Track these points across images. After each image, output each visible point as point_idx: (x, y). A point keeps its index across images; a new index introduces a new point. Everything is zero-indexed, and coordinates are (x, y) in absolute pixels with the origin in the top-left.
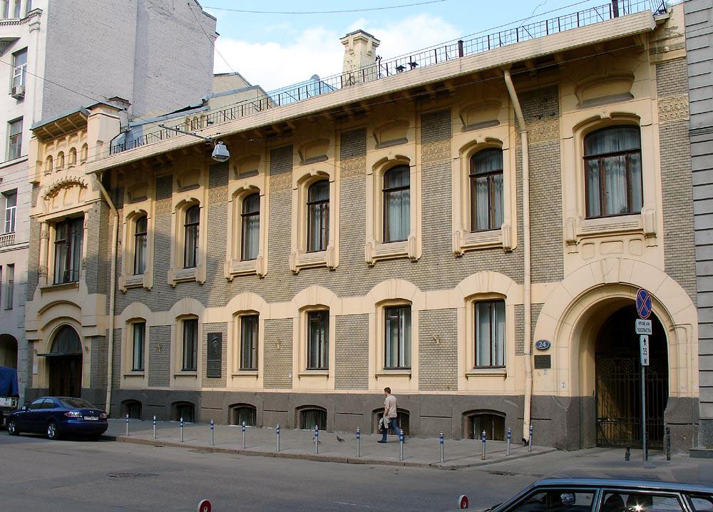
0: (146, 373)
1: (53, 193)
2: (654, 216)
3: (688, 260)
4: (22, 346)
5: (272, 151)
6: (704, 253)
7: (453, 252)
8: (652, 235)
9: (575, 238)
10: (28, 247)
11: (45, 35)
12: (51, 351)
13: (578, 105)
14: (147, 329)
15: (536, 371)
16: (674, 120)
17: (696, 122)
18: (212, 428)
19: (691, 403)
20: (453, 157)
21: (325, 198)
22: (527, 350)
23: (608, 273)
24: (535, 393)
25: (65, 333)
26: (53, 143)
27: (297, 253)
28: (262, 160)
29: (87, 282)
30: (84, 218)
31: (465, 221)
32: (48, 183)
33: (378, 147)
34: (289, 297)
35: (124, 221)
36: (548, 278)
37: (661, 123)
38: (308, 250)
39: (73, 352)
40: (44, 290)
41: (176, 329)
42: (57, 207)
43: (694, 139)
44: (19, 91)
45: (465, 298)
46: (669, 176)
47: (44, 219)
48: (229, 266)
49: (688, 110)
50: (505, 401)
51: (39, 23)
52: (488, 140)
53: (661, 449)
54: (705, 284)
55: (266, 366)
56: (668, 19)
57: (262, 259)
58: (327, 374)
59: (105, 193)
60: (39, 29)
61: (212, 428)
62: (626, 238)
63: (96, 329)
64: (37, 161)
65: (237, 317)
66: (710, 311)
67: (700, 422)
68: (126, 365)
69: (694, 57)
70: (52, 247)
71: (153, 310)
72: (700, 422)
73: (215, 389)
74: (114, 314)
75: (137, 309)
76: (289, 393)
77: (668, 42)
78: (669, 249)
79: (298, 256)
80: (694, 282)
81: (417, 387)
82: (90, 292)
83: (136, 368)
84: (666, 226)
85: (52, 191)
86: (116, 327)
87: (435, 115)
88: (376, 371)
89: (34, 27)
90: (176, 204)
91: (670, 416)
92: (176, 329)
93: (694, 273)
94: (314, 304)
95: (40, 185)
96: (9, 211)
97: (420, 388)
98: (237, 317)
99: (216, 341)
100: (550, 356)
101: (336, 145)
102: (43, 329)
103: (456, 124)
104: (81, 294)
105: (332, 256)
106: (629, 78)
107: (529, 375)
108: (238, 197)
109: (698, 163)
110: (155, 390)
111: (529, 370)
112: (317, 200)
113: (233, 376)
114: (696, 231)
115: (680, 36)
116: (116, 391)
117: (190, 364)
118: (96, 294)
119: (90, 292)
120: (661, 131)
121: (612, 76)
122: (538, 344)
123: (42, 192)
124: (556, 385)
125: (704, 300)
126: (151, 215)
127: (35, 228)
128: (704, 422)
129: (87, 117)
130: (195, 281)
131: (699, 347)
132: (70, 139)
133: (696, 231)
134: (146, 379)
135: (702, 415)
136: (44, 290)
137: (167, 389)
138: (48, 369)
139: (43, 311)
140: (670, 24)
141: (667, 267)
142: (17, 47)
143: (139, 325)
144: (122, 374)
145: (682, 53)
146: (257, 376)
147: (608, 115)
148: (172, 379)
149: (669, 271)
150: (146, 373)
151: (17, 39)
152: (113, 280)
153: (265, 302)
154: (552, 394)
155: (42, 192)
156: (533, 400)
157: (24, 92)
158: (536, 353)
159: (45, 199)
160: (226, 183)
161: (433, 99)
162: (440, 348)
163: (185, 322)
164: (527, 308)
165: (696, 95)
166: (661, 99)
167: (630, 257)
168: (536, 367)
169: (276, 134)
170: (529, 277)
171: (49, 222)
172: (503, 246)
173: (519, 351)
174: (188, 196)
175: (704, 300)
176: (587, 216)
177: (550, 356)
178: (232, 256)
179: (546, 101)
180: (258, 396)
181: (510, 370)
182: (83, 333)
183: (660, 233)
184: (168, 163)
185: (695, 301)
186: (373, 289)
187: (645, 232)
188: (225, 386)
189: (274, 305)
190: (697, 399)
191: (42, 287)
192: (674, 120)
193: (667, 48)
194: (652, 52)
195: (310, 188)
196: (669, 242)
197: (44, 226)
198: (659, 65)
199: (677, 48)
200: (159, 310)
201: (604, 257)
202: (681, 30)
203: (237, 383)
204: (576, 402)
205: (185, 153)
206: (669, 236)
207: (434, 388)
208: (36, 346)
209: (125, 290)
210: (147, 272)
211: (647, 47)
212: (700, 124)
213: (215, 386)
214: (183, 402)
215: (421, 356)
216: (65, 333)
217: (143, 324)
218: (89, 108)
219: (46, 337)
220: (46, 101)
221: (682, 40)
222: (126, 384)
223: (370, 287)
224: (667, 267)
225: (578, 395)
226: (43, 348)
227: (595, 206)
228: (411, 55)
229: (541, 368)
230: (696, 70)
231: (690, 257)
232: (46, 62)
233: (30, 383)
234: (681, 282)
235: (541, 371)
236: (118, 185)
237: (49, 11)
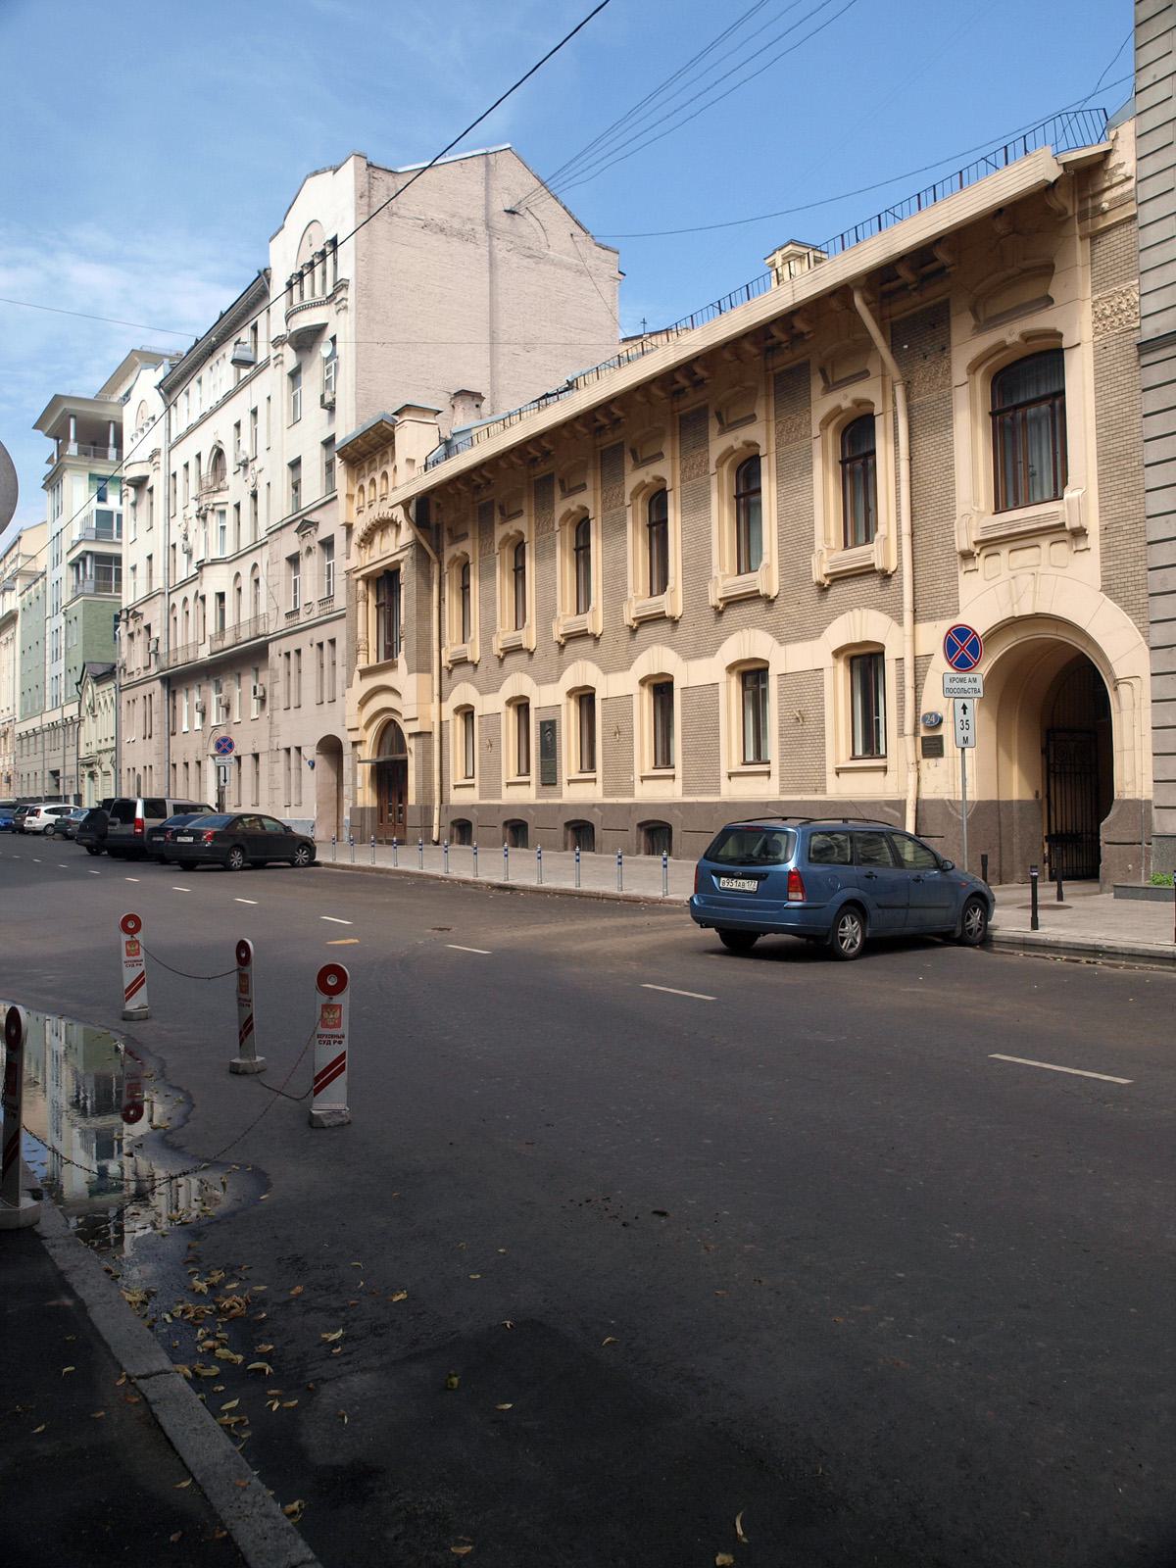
0: (678, 771)
1: (367, 539)
2: (1082, 503)
3: (1137, 568)
4: (347, 749)
5: (681, 418)
6: (1163, 555)
7: (958, 550)
8: (1079, 533)
9: (972, 547)
10: (343, 616)
11: (353, 314)
12: (378, 755)
13: (975, 327)
14: (476, 719)
15: (924, 762)
16: (1116, 331)
17: (1151, 329)
18: (421, 850)
19: (1141, 808)
20: (814, 436)
21: (1056, 389)
22: (909, 728)
23: (1018, 600)
24: (924, 796)
25: (390, 732)
26: (363, 467)
27: (825, 551)
28: (759, 395)
29: (406, 658)
30: (399, 570)
31: (832, 534)
32: (360, 526)
33: (722, 432)
34: (817, 633)
35: (445, 571)
36: (939, 614)
37: (1097, 338)
38: (846, 545)
39: (400, 756)
40: (365, 673)
41: (641, 701)
42: (374, 557)
43: (1147, 359)
44: (328, 399)
45: (568, 693)
46: (1108, 428)
47: (358, 575)
48: (821, 561)
49: (1137, 310)
50: (887, 809)
51: (346, 300)
52: (1027, 337)
53: (1098, 882)
54: (1165, 607)
55: (605, 765)
56: (1107, 154)
57: (768, 566)
58: (767, 769)
59: (418, 533)
60: (345, 308)
61: (421, 850)
62: (1045, 543)
63: (418, 722)
64: (347, 495)
65: (735, 673)
66: (1170, 652)
67: (1153, 840)
68: (456, 775)
69: (1148, 213)
70: (372, 612)
71: (482, 693)
72: (1153, 840)
73: (551, 801)
74: (915, 622)
75: (464, 693)
76: (717, 803)
77: (1108, 195)
78: (1107, 552)
79: (828, 553)
80: (1145, 605)
81: (777, 790)
82: (410, 672)
83: (750, 757)
84: (1104, 514)
85: (369, 529)
86: (920, 652)
87: (790, 372)
88: (837, 762)
89: (340, 306)
90: (631, 490)
91: (1110, 829)
92: (641, 701)
93: (1144, 591)
94: (656, 673)
95: (354, 527)
96: (329, 565)
97: (782, 792)
98: (735, 673)
99: (549, 728)
100: (941, 736)
101: (768, 395)
102: (367, 726)
103: (961, 327)
104: (401, 677)
105: (768, 578)
106: (1047, 270)
107: (913, 768)
108: (455, 566)
109: (1153, 400)
110: (693, 803)
111: (912, 759)
112: (856, 454)
113: (730, 776)
114: (1149, 517)
115: (1129, 179)
116: (445, 807)
117: (871, 740)
118: (415, 674)
119: (410, 672)
120: (1096, 353)
121: (1025, 271)
122: (925, 719)
123: (355, 538)
124: (951, 782)
125: (1161, 635)
126: (768, 448)
127: (350, 589)
128: (1160, 840)
129: (393, 427)
130: (467, 661)
131: (1152, 715)
132: (381, 461)
133: (1149, 517)
134: (679, 782)
135: (1157, 829)
136: (365, 673)
137: (558, 801)
138: (375, 783)
139: (364, 702)
140: (1113, 161)
141: (1106, 583)
142: (329, 334)
143: (467, 713)
144: (452, 783)
145: (1131, 210)
146: (768, 773)
147: (1016, 338)
148: (831, 777)
149: (1108, 589)
150: (678, 771)
151: (325, 326)
152: (436, 654)
153: (776, 642)
154: (946, 797)
155: (355, 538)
156: (919, 807)
157: (334, 399)
158: (923, 733)
159: (359, 546)
160: (807, 405)
161: (787, 348)
162: (805, 726)
163: (852, 661)
164: (909, 663)
165: (1152, 281)
166: (1096, 297)
167: (1052, 570)
168: (925, 756)
169: (780, 343)
170: (911, 615)
171: (367, 579)
172: (877, 567)
173: (901, 733)
174: (846, 397)
175: (1161, 635)
176: (996, 509)
177: (941, 736)
178: (827, 540)
179: (934, 328)
180: (596, 810)
181: (891, 762)
182: (407, 728)
183: (1094, 527)
184: (797, 338)
185: (1146, 635)
186: (723, 645)
187: (1068, 527)
188: (560, 795)
189: (612, 677)
190: (1149, 802)
191: (360, 668)
192: (1116, 331)
193: (1105, 205)
194: (1083, 216)
195: (738, 473)
196: (1108, 541)
197: (361, 585)
198: (1095, 237)
199: (1120, 202)
200: (698, 656)
201: (1014, 573)
202: (1129, 168)
203: (578, 792)
204: (372, 808)
205: (727, 355)
206: (1107, 531)
207: (799, 791)
208: (359, 749)
209: (450, 666)
210: (473, 640)
211: (1072, 209)
212: (1157, 330)
213: (550, 797)
214: (653, 821)
215: (782, 744)
216: (390, 732)
217: (592, 696)
218: (396, 414)
219: (370, 736)
220: (359, 407)
221: (1131, 184)
222: (458, 797)
223: (719, 644)
224: (1106, 583)
225: (995, 798)
226: (367, 752)
227: (1010, 489)
228: (1023, 133)
229: (930, 757)
230: (1153, 235)
231: (1140, 563)
232: (357, 353)
233: (355, 803)
234: (1128, 606)
235: (932, 761)
236: (437, 520)
237: (356, 279)
